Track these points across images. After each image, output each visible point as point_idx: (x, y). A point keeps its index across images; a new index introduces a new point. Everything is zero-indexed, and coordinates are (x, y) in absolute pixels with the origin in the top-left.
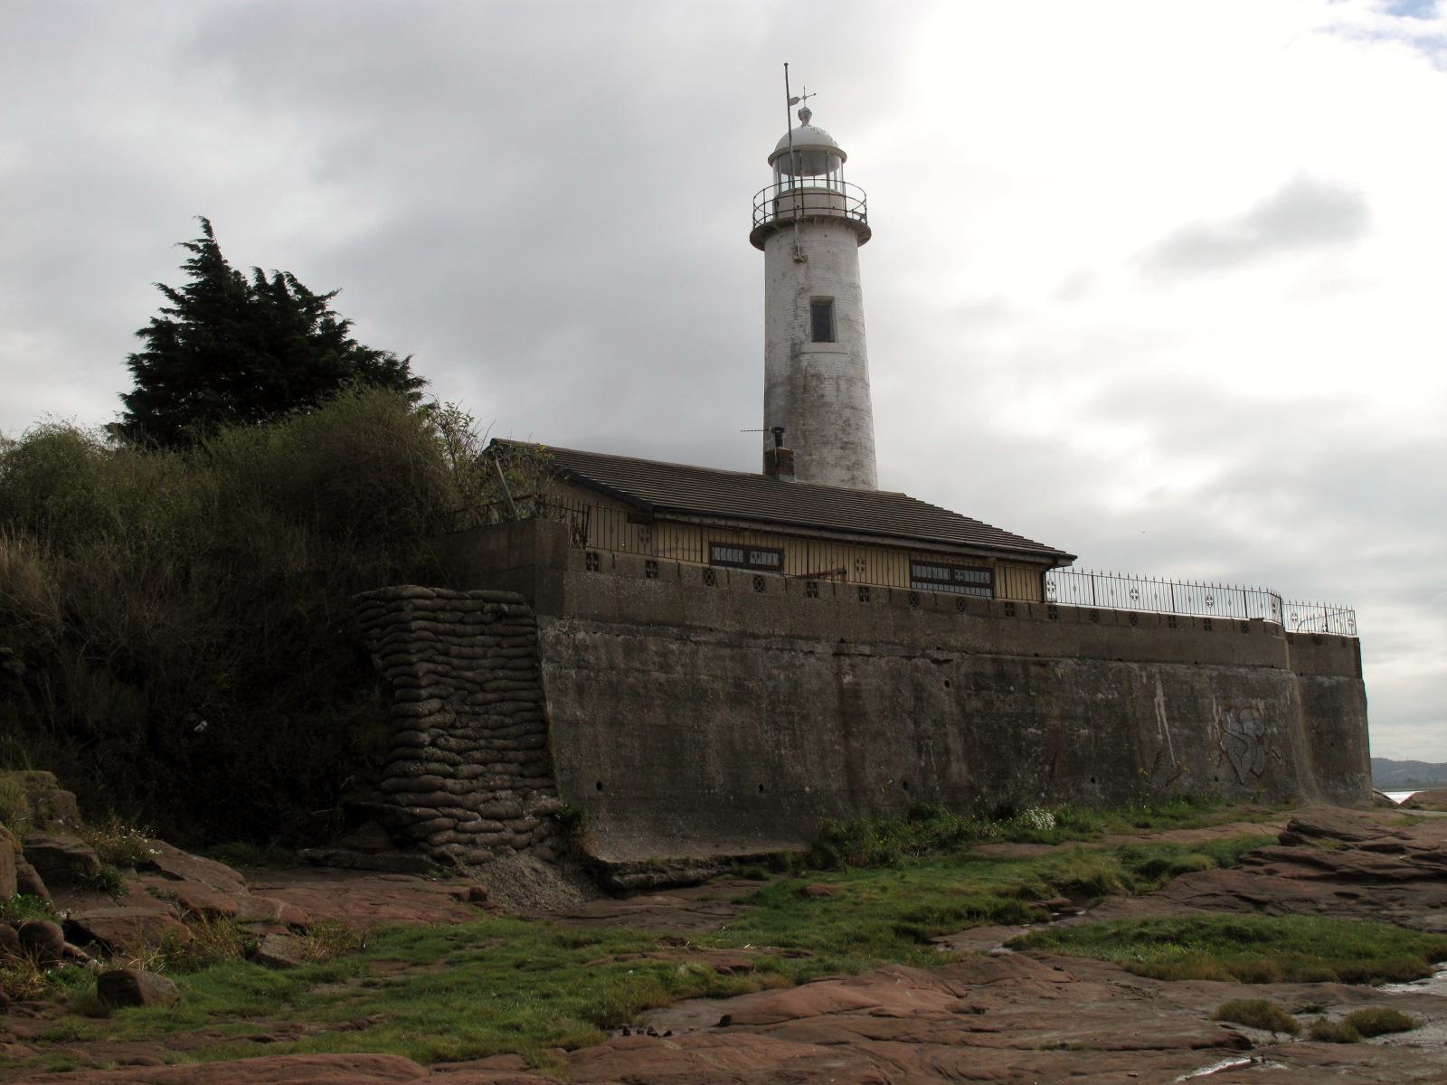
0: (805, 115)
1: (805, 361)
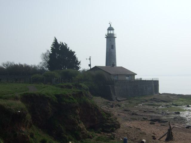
0: (110, 25)
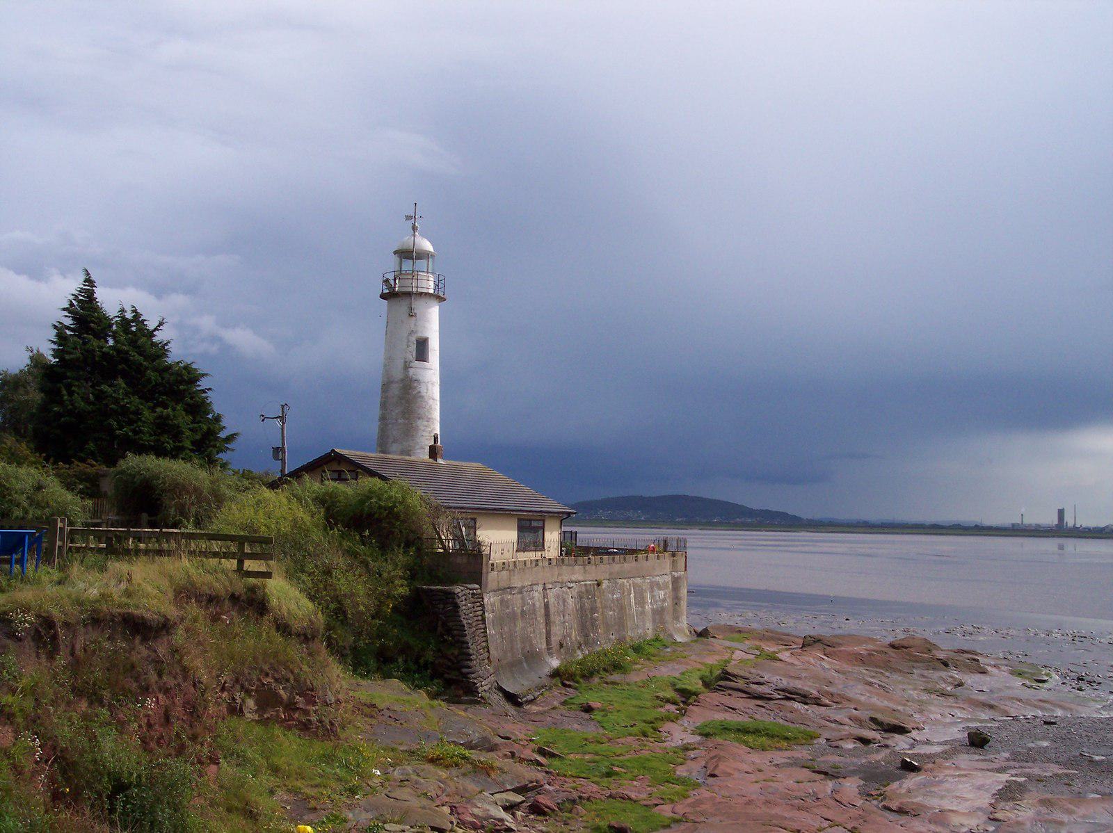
1: (411, 372)
